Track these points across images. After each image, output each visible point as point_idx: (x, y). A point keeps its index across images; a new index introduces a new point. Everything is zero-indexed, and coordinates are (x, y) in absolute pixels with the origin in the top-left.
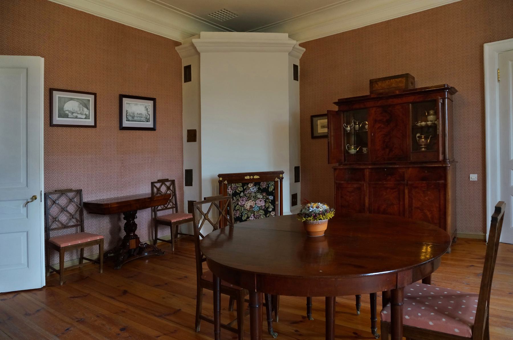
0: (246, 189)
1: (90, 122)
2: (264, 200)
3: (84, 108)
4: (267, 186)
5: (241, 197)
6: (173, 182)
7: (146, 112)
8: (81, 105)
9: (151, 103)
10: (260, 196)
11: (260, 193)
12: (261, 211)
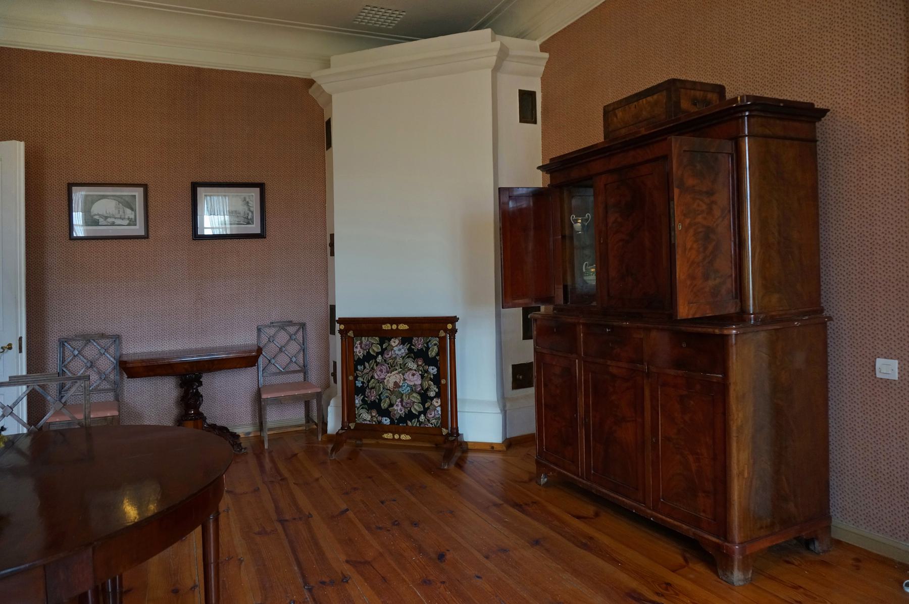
0: (386, 349)
1: (138, 229)
2: (420, 373)
3: (127, 209)
4: (425, 345)
5: (377, 364)
6: (303, 326)
7: (246, 208)
8: (121, 205)
9: (255, 193)
10: (412, 365)
11: (412, 358)
12: (414, 395)
